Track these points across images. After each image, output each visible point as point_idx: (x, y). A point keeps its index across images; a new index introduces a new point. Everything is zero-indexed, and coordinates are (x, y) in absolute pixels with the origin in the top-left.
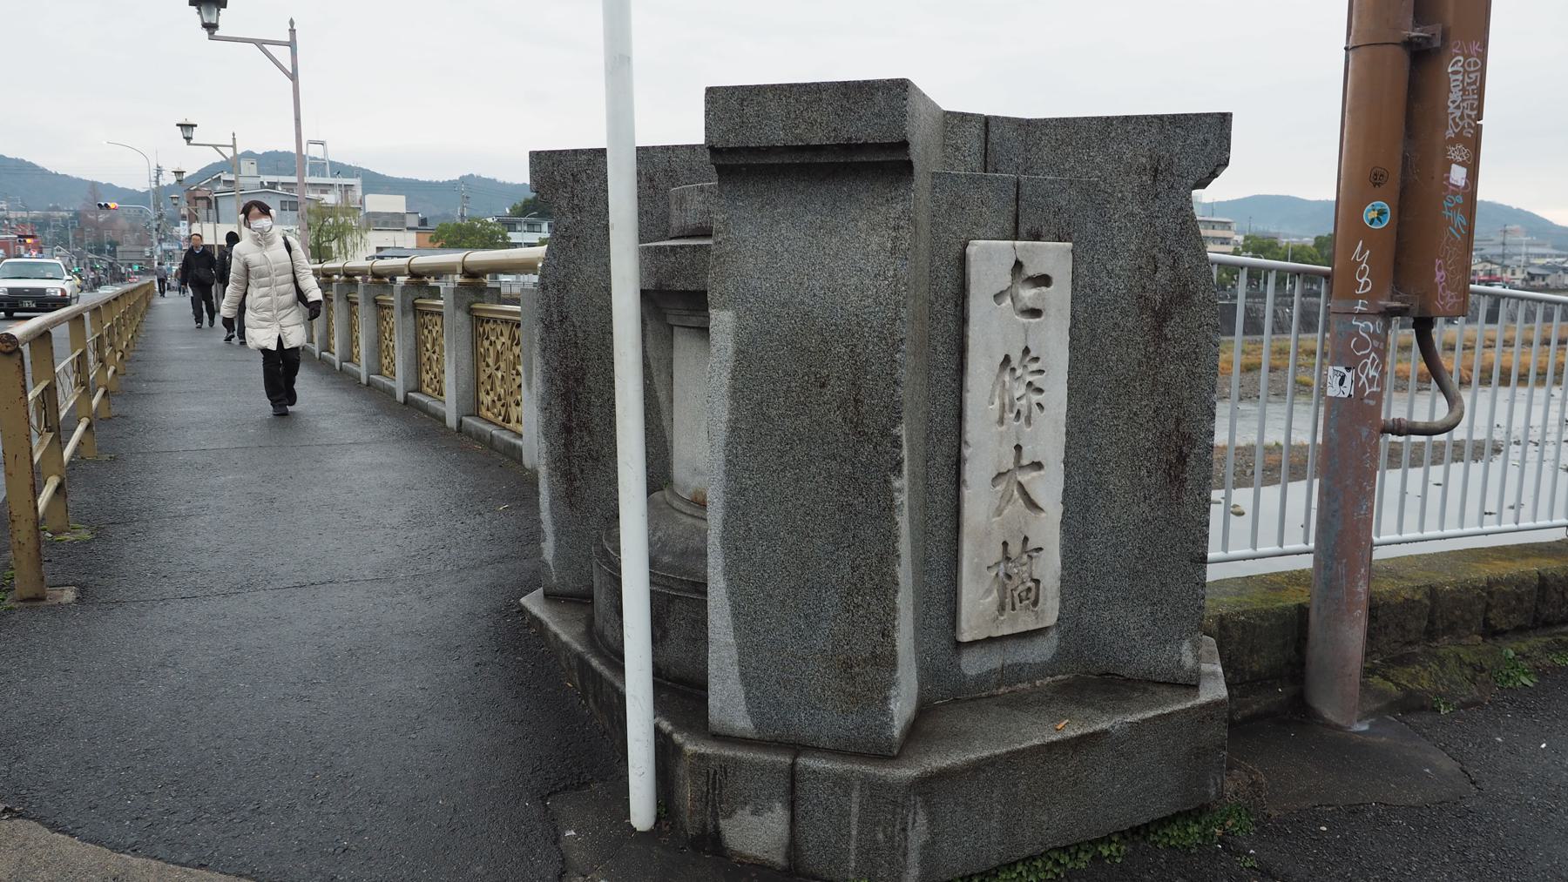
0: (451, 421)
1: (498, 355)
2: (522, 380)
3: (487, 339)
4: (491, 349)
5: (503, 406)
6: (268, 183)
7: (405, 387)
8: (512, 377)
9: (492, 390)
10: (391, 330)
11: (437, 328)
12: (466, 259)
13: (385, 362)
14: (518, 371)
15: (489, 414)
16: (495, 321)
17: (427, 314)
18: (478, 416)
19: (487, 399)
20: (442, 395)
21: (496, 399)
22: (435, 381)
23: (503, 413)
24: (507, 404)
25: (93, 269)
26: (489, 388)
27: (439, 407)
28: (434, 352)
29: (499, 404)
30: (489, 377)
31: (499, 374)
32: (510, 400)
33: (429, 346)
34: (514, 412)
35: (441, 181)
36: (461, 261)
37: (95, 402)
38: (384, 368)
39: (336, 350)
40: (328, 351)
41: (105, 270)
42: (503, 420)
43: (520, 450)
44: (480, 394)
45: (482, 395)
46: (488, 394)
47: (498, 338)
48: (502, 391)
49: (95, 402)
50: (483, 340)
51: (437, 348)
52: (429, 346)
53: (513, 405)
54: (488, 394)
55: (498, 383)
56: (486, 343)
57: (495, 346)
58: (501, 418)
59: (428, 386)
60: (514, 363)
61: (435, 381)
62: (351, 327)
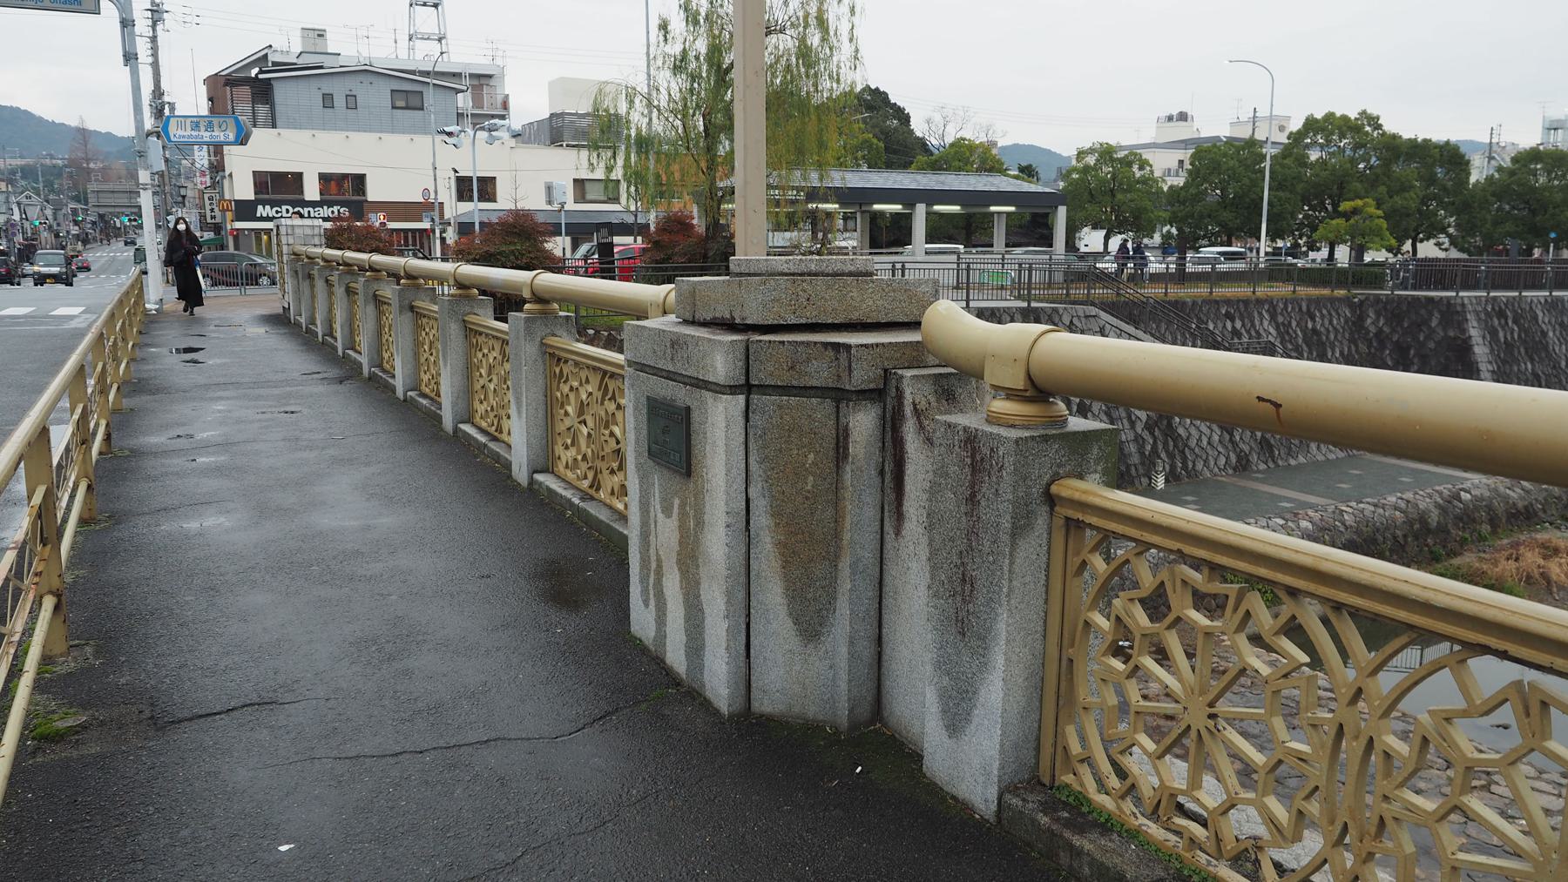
0: (400, 393)
1: (490, 369)
2: (510, 396)
3: (480, 350)
4: (572, 396)
5: (496, 416)
6: (325, 179)
7: (455, 414)
8: (603, 438)
9: (485, 399)
10: (390, 326)
11: (495, 354)
12: (535, 281)
13: (386, 356)
14: (566, 412)
15: (427, 390)
16: (487, 335)
17: (424, 316)
18: (553, 472)
19: (481, 408)
20: (439, 396)
21: (580, 457)
22: (433, 382)
23: (496, 423)
24: (500, 413)
25: (76, 223)
26: (569, 441)
27: (502, 453)
28: (431, 354)
29: (492, 415)
30: (483, 387)
31: (492, 386)
32: (503, 413)
33: (426, 347)
34: (505, 424)
35: (1338, 114)
36: (529, 282)
37: (111, 397)
38: (424, 385)
39: (338, 335)
40: (353, 349)
41: (94, 223)
42: (496, 431)
43: (511, 463)
44: (556, 447)
45: (477, 405)
46: (481, 403)
47: (581, 384)
48: (589, 451)
49: (111, 397)
50: (559, 382)
51: (434, 351)
52: (426, 347)
53: (504, 418)
54: (481, 403)
55: (491, 395)
56: (480, 355)
57: (488, 360)
58: (494, 428)
59: (481, 418)
60: (607, 422)
61: (433, 382)
62: (313, 297)
